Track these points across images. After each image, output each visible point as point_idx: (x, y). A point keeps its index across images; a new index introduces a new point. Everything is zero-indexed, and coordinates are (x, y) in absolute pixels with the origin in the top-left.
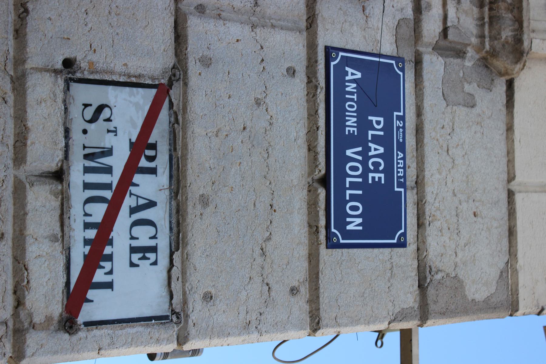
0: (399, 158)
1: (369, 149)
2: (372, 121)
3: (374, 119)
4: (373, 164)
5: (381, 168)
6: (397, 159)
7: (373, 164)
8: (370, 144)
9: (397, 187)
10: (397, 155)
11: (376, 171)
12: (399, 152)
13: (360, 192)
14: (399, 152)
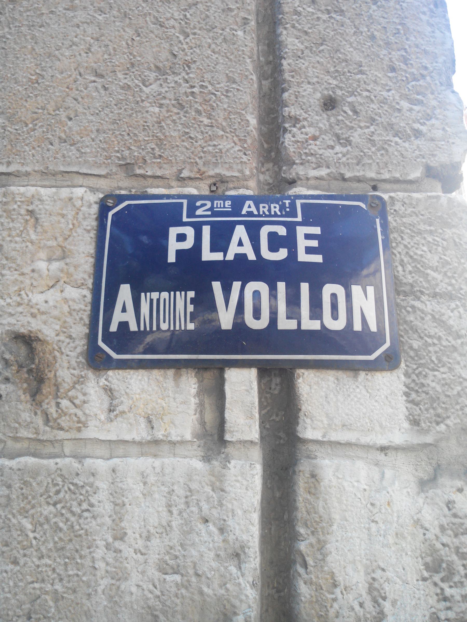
0: (256, 213)
1: (241, 258)
2: (179, 253)
3: (173, 246)
4: (273, 248)
5: (282, 231)
6: (259, 216)
7: (273, 248)
8: (230, 256)
9: (296, 217)
10: (250, 214)
11: (290, 241)
12: (244, 212)
13: (378, 221)
14: (244, 212)
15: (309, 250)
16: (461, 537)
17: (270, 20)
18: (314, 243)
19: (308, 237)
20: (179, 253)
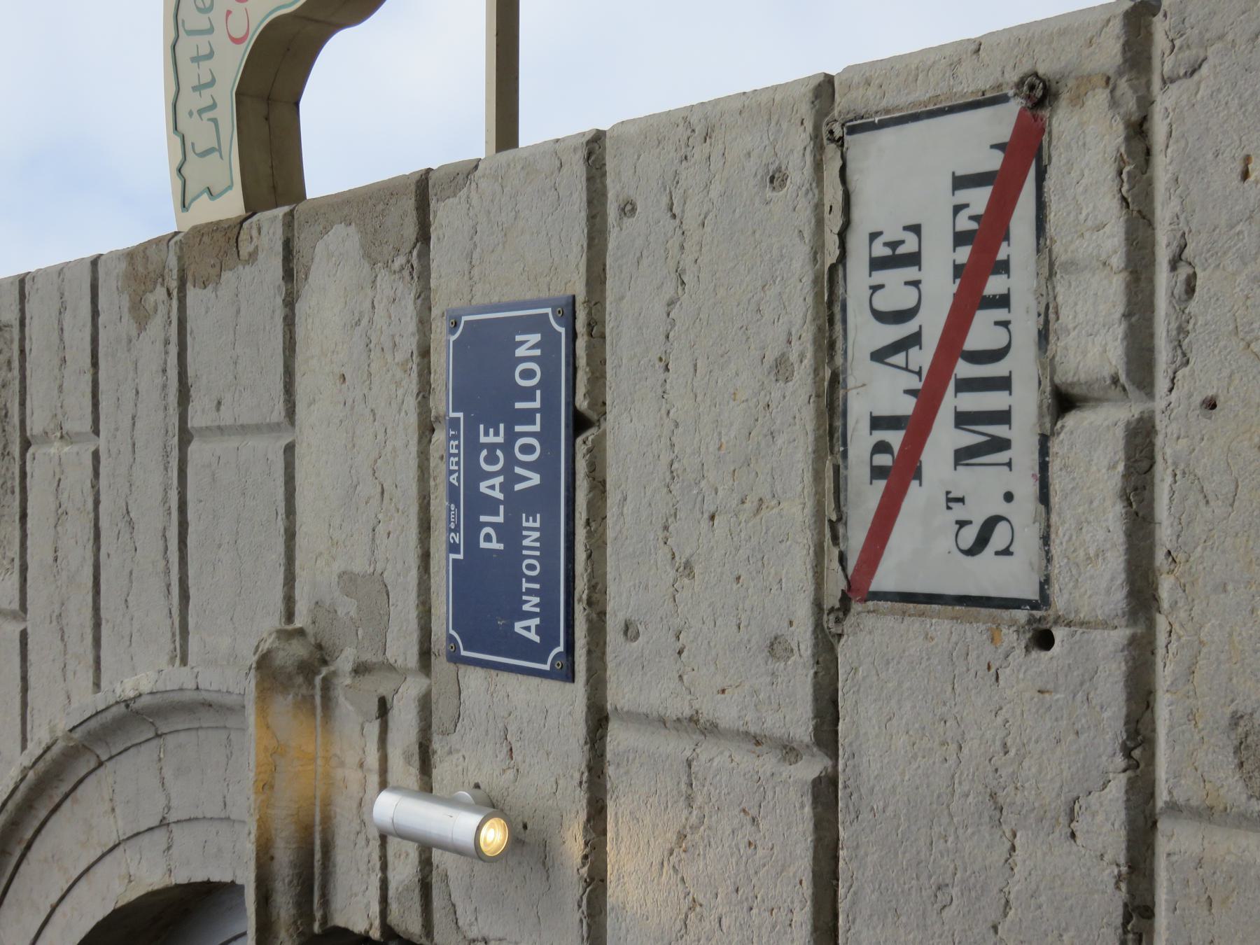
2: (498, 541)
3: (495, 545)
5: (484, 453)
6: (459, 471)
8: (501, 496)
11: (492, 447)
15: (535, 521)
16: (1120, 635)
17: (1139, 911)
18: (491, 431)
19: (487, 434)
20: (498, 541)
